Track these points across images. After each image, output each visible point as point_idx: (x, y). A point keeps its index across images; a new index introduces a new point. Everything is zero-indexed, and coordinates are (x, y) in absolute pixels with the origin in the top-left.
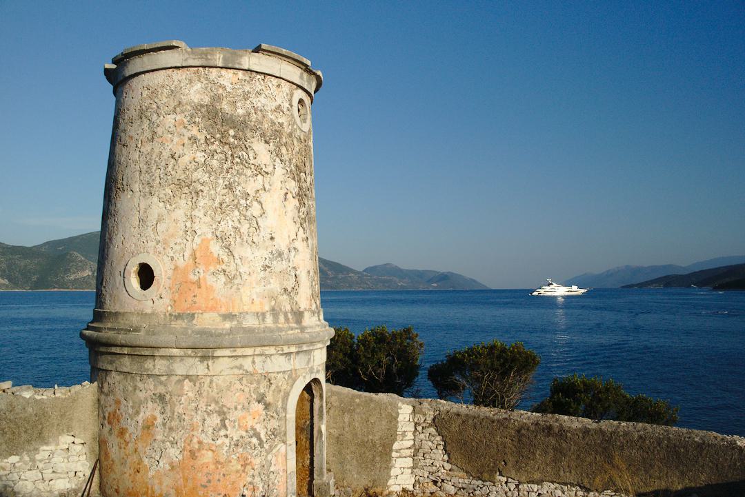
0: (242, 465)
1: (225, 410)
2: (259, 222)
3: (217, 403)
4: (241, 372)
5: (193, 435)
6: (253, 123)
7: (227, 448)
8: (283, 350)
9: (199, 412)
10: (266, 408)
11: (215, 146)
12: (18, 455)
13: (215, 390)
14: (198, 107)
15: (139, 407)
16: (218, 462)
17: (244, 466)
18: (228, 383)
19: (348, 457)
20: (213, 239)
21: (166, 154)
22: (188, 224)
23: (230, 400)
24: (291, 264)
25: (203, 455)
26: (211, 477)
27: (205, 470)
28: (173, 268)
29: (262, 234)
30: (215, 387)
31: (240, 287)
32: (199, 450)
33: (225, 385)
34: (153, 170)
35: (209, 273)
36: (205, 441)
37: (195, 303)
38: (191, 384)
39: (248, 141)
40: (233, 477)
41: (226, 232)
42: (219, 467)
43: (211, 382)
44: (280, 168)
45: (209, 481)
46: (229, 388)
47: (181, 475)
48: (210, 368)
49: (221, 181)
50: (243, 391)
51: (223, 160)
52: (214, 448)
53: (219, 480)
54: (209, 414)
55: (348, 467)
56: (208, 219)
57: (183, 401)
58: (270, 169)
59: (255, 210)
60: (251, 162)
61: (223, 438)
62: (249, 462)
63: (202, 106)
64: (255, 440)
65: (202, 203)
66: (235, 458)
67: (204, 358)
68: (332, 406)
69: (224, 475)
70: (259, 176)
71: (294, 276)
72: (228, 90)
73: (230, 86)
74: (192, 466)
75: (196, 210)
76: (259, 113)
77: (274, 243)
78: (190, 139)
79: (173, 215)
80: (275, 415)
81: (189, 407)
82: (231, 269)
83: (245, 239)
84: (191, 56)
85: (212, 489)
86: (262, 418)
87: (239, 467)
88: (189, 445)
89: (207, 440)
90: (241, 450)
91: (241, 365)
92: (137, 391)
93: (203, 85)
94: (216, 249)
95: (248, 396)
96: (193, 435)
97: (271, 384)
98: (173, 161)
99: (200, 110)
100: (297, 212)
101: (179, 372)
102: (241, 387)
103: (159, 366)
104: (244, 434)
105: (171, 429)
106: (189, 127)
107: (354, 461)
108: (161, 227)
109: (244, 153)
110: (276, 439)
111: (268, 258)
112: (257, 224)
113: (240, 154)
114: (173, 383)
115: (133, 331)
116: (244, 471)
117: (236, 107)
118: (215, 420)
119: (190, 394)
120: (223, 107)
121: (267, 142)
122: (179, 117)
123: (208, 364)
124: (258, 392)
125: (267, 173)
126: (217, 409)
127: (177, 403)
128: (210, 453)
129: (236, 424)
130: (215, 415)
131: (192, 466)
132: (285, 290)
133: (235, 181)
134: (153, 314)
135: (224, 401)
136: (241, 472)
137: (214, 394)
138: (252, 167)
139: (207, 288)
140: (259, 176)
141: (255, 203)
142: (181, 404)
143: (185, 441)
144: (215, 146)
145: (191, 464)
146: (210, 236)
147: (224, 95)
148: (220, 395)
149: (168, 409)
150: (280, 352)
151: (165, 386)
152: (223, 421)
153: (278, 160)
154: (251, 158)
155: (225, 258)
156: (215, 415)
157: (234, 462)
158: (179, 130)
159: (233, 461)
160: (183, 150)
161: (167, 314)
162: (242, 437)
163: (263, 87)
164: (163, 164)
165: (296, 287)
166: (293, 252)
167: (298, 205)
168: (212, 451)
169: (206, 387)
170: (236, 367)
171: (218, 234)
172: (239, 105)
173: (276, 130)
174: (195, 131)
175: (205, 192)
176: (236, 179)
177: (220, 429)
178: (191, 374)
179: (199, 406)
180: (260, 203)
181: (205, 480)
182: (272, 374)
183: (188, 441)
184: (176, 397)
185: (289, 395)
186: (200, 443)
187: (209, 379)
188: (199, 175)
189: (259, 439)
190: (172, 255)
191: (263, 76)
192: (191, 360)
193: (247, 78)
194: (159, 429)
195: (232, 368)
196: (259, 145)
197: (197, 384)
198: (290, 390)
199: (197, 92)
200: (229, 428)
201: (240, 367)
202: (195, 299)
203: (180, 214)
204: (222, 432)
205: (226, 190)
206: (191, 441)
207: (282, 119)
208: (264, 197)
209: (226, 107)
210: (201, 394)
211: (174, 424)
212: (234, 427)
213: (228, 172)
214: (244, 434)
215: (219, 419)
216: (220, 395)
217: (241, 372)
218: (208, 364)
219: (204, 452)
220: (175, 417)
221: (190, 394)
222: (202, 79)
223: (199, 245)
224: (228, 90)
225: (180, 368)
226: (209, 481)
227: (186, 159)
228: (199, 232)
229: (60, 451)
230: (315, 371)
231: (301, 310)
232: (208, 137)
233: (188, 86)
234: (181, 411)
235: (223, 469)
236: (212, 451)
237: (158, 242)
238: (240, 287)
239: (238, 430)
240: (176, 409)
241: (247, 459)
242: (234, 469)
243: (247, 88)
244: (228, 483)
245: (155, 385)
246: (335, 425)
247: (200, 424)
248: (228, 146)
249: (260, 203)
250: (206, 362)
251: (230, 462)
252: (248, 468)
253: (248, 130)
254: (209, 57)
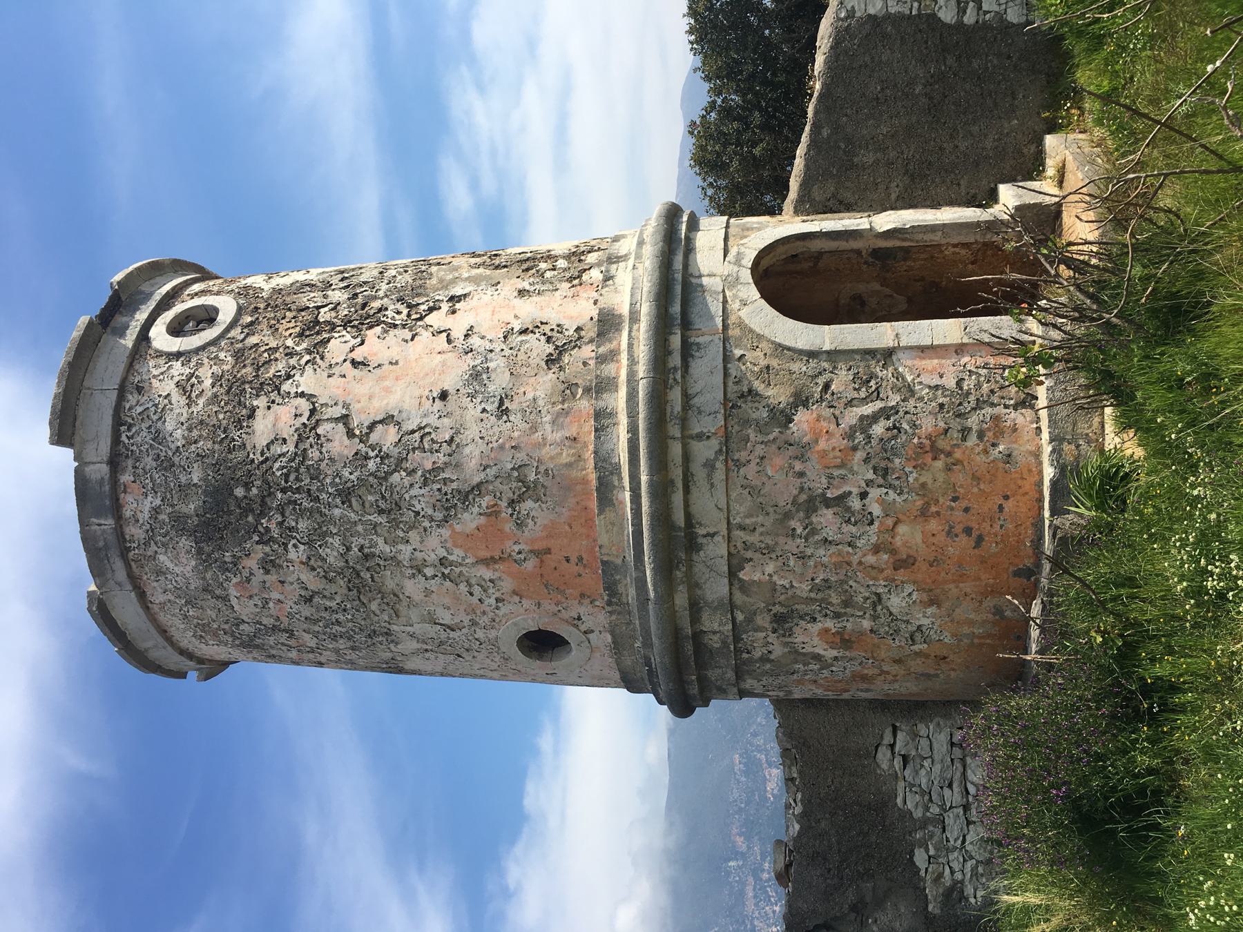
0: (935, 459)
1: (803, 497)
2: (410, 428)
3: (787, 516)
4: (720, 465)
5: (860, 563)
6: (217, 447)
7: (891, 492)
8: (675, 369)
9: (809, 551)
10: (805, 404)
11: (271, 523)
12: (912, 851)
13: (760, 519)
14: (205, 560)
15: (804, 654)
16: (924, 513)
17: (936, 452)
18: (746, 492)
19: (963, 145)
20: (451, 526)
21: (307, 611)
22: (429, 572)
23: (784, 490)
24: (498, 346)
25: (905, 544)
26: (958, 529)
27: (941, 538)
28: (517, 599)
29: (432, 420)
30: (753, 520)
31: (542, 469)
32: (893, 552)
33: (749, 498)
34: (343, 630)
35: (519, 533)
36: (874, 539)
37: (580, 559)
38: (748, 567)
39: (251, 456)
40: (960, 478)
41: (433, 500)
42: (934, 509)
43: (742, 528)
44: (302, 380)
45: (968, 531)
46: (753, 491)
47: (952, 586)
48: (712, 530)
49: (337, 512)
50: (762, 458)
51: (294, 509)
52: (890, 522)
53: (967, 510)
54: (814, 532)
55: (989, 143)
56: (413, 535)
57: (786, 583)
58: (304, 405)
59: (387, 437)
60: (292, 449)
61: (866, 501)
62: (927, 442)
63: (200, 552)
64: (878, 429)
65: (382, 547)
66: (914, 475)
67: (692, 545)
68: (834, 196)
69: (955, 499)
70: (320, 431)
71: (523, 337)
72: (158, 502)
73: (149, 498)
74: (931, 566)
75: (400, 558)
76: (195, 433)
77: (452, 391)
78: (267, 572)
79: (418, 596)
80: (821, 381)
81: (798, 570)
82: (507, 490)
83: (447, 459)
84: (109, 576)
85: (986, 525)
86: (828, 412)
87: (939, 464)
88: (882, 571)
89: (872, 534)
90: (897, 461)
91: (705, 465)
92: (772, 657)
93: (159, 550)
94: (470, 520)
95: (774, 447)
96: (860, 563)
97: (750, 391)
98: (316, 600)
99: (209, 555)
100: (392, 332)
101: (725, 590)
102: (753, 464)
103: (715, 625)
104: (860, 455)
105: (847, 603)
106: (246, 573)
107: (975, 129)
108: (446, 618)
109: (277, 465)
110: (880, 374)
111: (483, 405)
112: (413, 432)
113: (278, 474)
114: (748, 599)
115: (650, 666)
116: (949, 454)
117: (190, 485)
118: (826, 519)
119: (770, 568)
120: (192, 511)
121: (251, 416)
122: (233, 592)
123: (705, 536)
124: (766, 424)
125: (313, 412)
126: (802, 514)
127: (790, 593)
128: (902, 529)
129: (836, 473)
130: (814, 519)
131: (931, 566)
132: (550, 361)
133: (333, 484)
134: (612, 633)
135: (784, 500)
136: (950, 460)
137: (769, 521)
138: (302, 447)
139: (549, 536)
140: (320, 431)
141: (374, 438)
142: (792, 586)
143: (875, 579)
144: (271, 523)
145: (924, 567)
146: (446, 533)
147: (170, 510)
148: (771, 510)
149: (801, 608)
150: (679, 376)
151: (755, 614)
152: (828, 503)
153: (286, 387)
154: (285, 450)
155: (486, 501)
156: (814, 519)
157: (926, 478)
158: (256, 591)
159: (922, 480)
160: (292, 584)
161: (609, 609)
162: (867, 460)
163: (144, 426)
164: (326, 615)
165: (547, 329)
166: (475, 341)
167: (378, 329)
168: (896, 524)
169: (752, 539)
170: (710, 476)
171: (439, 516)
172: (183, 479)
173: (228, 392)
174: (252, 563)
175: (363, 542)
176: (328, 481)
177: (848, 509)
178: (726, 568)
179: (795, 551)
180: (372, 427)
181: (963, 540)
182: (729, 389)
183: (874, 573)
184: (778, 594)
185: (780, 345)
186: (876, 549)
187: (737, 533)
188: (332, 553)
189: (874, 418)
190: (493, 601)
191: (123, 428)
192: (699, 568)
193: (130, 462)
194: (849, 626)
195: (712, 485)
196: (257, 434)
197: (749, 554)
198: (768, 340)
199: (176, 559)
200: (846, 488)
201: (710, 466)
202: (574, 559)
203: (413, 588)
204: (856, 504)
205: (353, 500)
206: (873, 567)
207: (206, 375)
208: (359, 420)
209: (192, 507)
210: (768, 547)
211: (835, 599)
212: (843, 478)
213: (317, 499)
214: (860, 455)
215: (825, 511)
216: (771, 510)
217: (720, 465)
218: (705, 536)
219: (898, 541)
220: (820, 596)
221: (770, 568)
222: (149, 553)
223: (466, 551)
224: (158, 502)
225: (716, 588)
226: (968, 531)
227: (306, 576)
228: (442, 553)
229: (907, 773)
230: (736, 268)
231: (595, 313)
232: (256, 538)
233: (169, 577)
234: (805, 587)
235: (941, 500)
236: (896, 524)
237: (474, 623)
238: (542, 469)
239: (851, 470)
240: (805, 595)
241: (921, 446)
242: (941, 477)
243: (149, 462)
244: (975, 490)
245: (756, 630)
246: (882, 187)
247: (833, 549)
248: (268, 500)
249: (372, 427)
250: (700, 540)
251: (923, 485)
252: (942, 444)
253: (230, 456)
254: (101, 544)
